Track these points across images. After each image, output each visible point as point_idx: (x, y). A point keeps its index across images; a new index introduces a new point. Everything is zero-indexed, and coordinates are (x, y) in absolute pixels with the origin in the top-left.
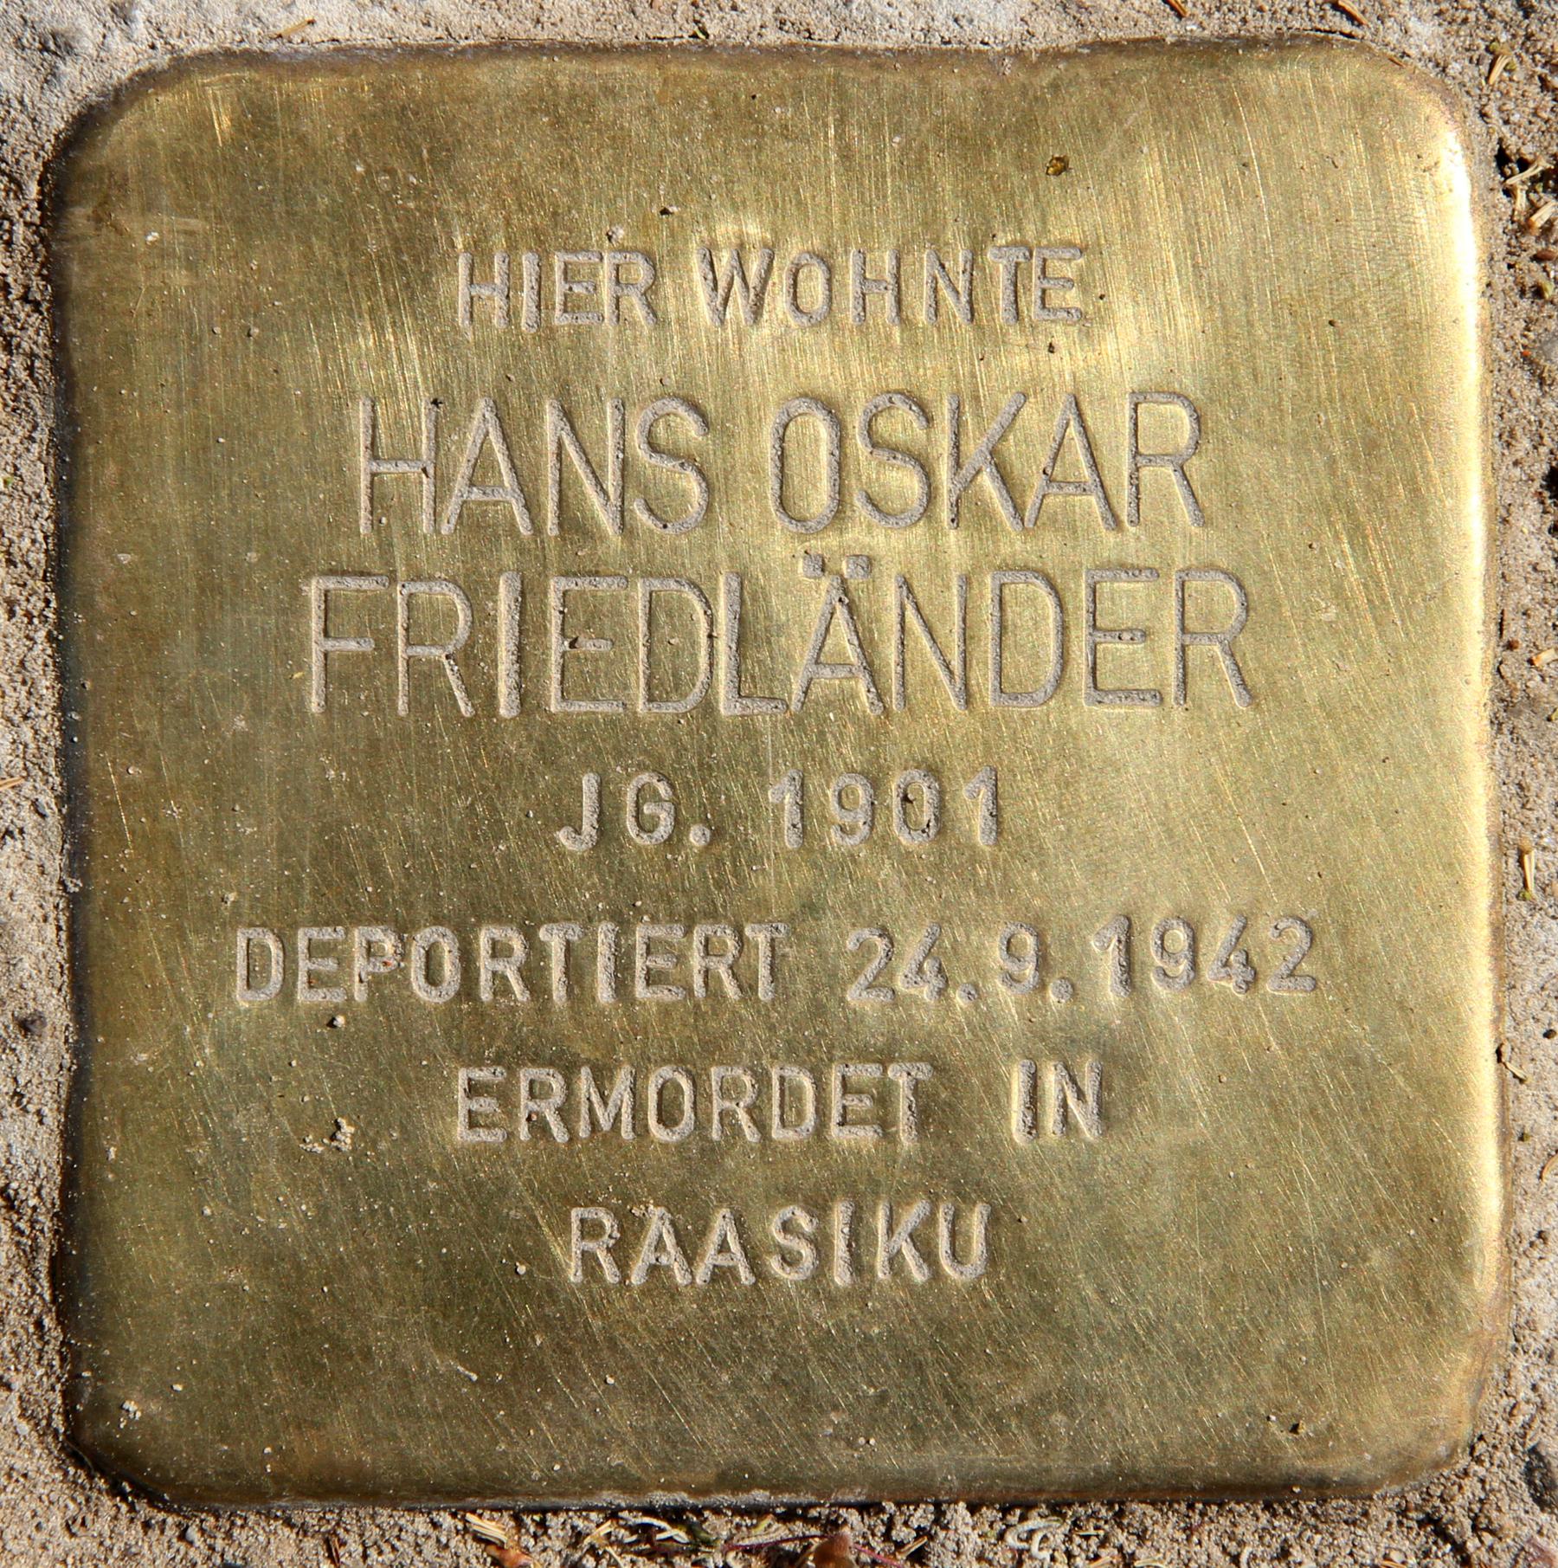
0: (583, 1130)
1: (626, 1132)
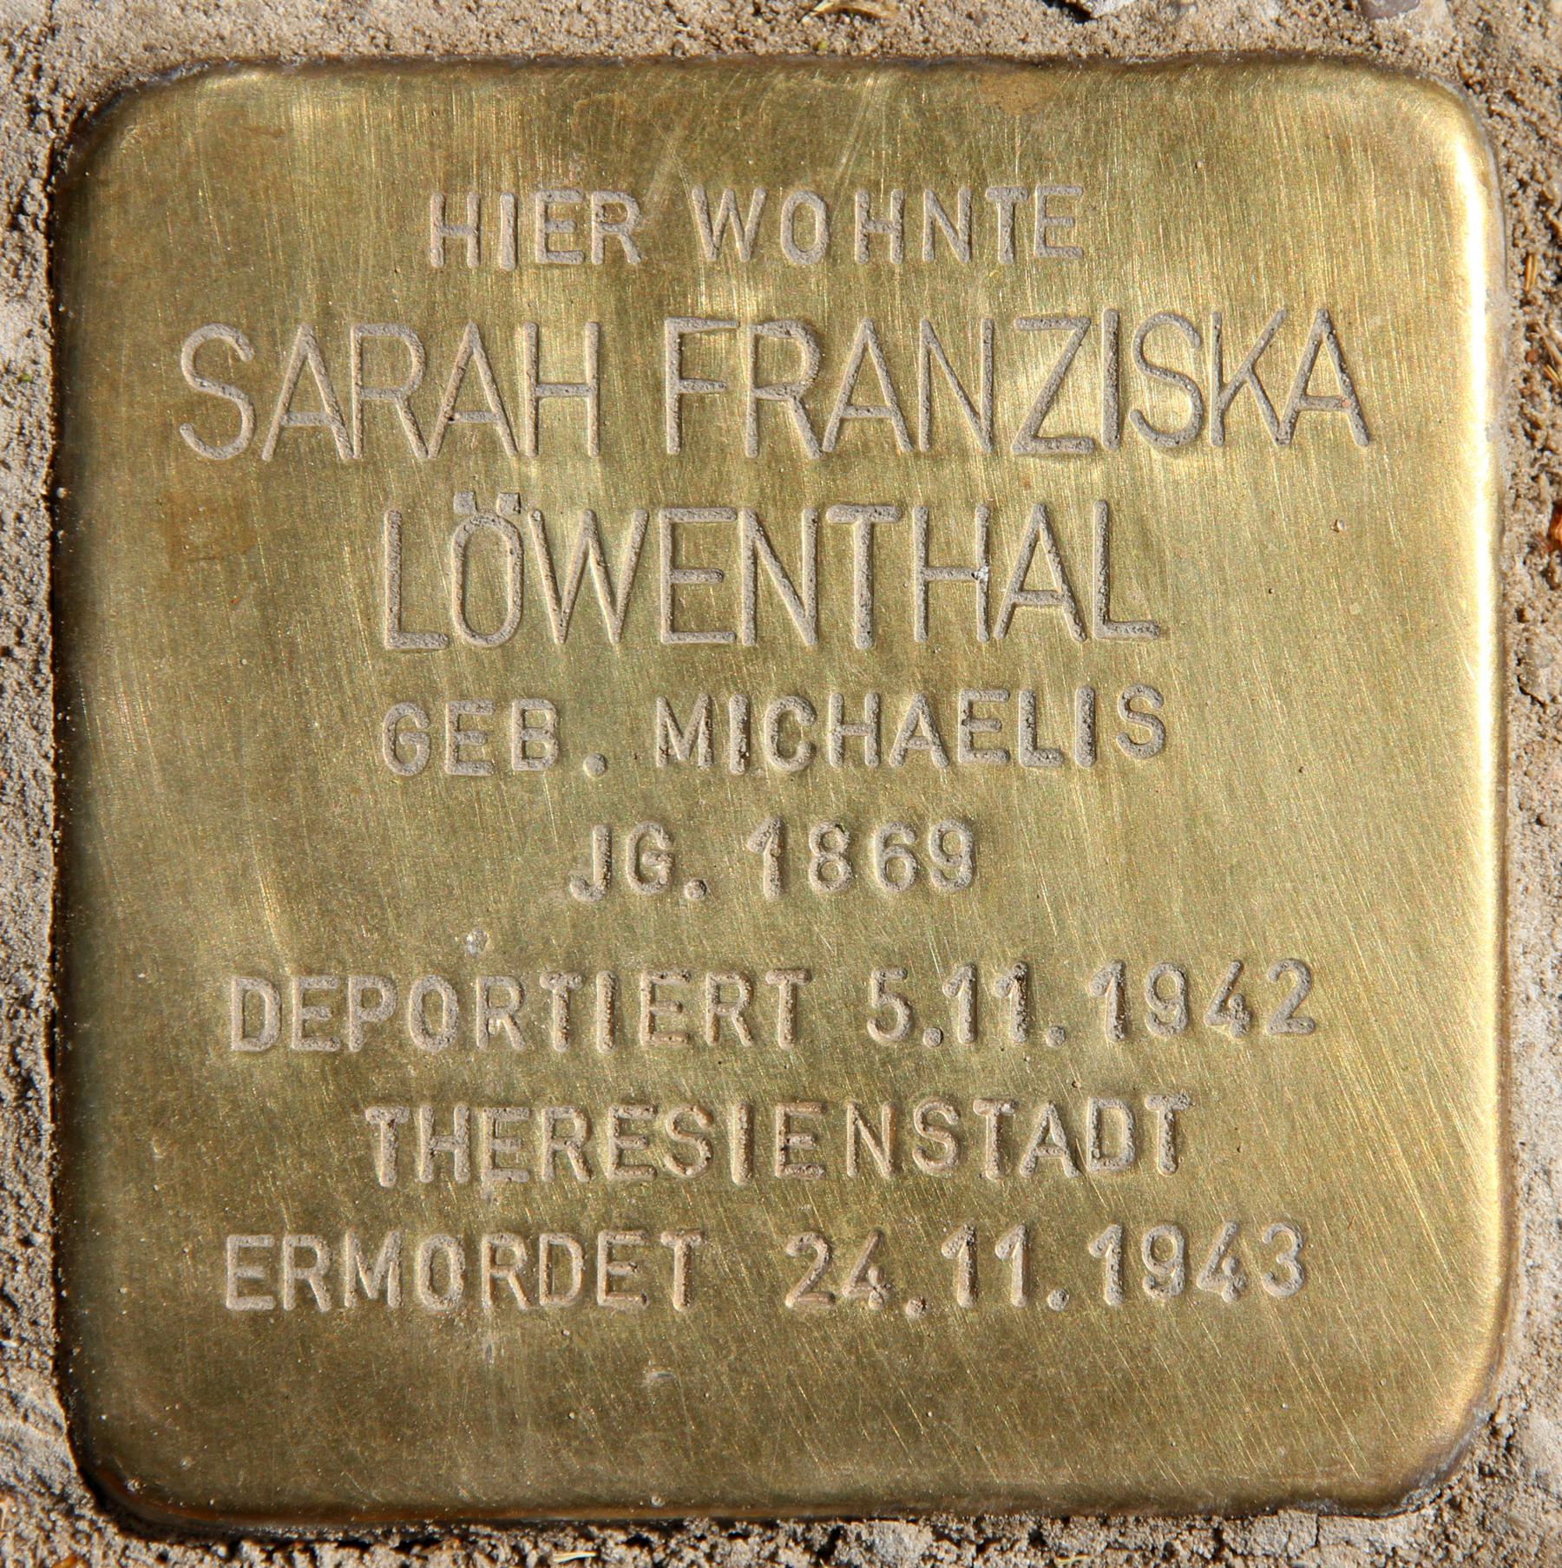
0: (348, 1299)
1: (392, 1301)
